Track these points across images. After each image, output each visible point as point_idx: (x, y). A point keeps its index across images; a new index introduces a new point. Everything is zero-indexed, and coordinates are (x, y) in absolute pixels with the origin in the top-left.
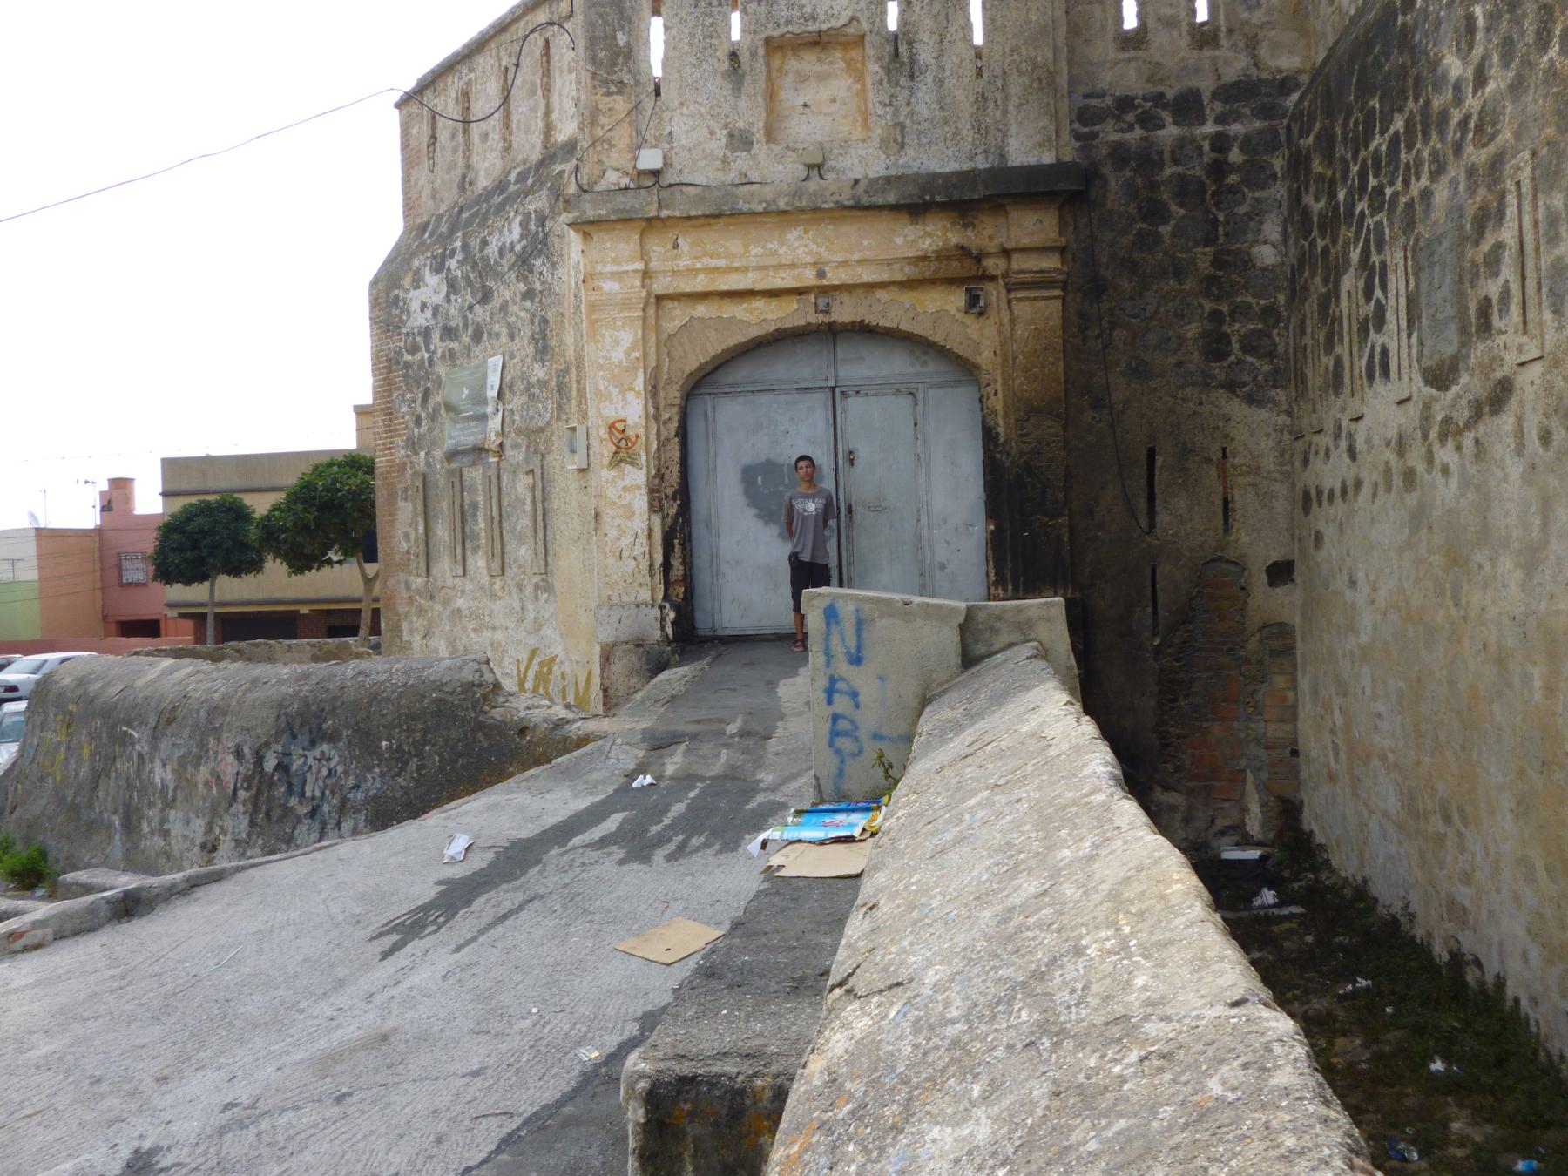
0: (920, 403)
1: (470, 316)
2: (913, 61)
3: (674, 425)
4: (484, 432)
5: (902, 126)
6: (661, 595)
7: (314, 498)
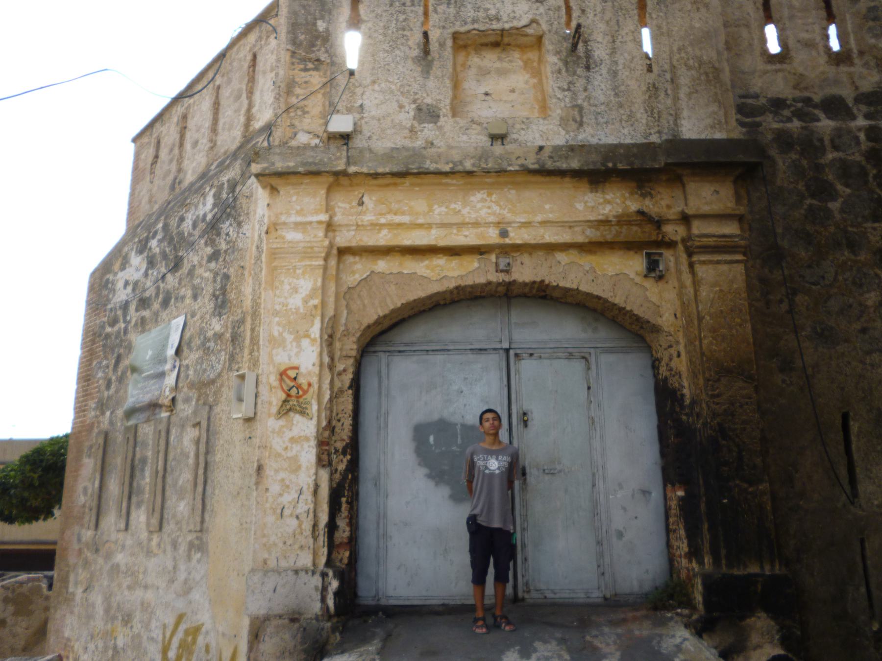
0: (593, 367)
1: (162, 285)
2: (588, 55)
3: (348, 377)
4: (161, 388)
5: (580, 108)
6: (323, 560)
7: (42, 461)
